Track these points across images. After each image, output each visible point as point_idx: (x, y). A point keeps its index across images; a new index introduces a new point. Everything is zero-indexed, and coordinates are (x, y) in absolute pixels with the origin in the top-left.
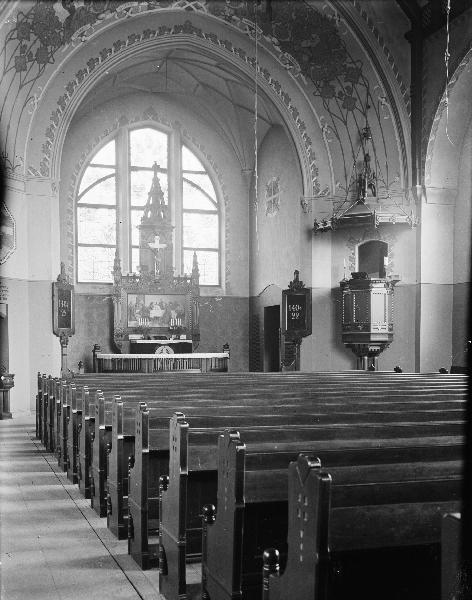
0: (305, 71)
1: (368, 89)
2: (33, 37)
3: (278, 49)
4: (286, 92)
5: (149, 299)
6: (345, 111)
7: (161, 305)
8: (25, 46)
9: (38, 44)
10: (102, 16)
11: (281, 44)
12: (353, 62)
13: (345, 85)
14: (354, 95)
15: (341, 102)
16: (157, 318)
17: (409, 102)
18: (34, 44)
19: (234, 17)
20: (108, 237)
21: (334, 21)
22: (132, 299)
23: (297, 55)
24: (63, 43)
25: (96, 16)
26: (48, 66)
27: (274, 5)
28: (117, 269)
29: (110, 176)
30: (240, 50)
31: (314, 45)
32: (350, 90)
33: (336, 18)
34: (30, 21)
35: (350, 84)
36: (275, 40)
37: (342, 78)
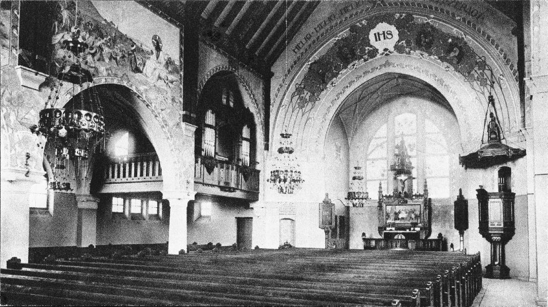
0: (456, 69)
1: (492, 71)
2: (306, 92)
3: (439, 61)
4: (416, 66)
5: (398, 208)
6: (482, 87)
7: (405, 211)
8: (302, 97)
9: (309, 94)
10: (340, 73)
11: (440, 58)
12: (480, 58)
13: (479, 72)
14: (485, 77)
15: (479, 83)
16: (403, 218)
17: (517, 74)
18: (307, 95)
19: (412, 52)
20: (383, 175)
21: (463, 38)
22: (389, 208)
23: (450, 62)
24: (323, 90)
25: (338, 74)
26: (317, 102)
27: (414, 194)
28: (380, 192)
29: (384, 143)
30: (426, 70)
31: (457, 54)
32: (482, 74)
33: (464, 36)
34: (303, 86)
35: (481, 71)
36: (436, 57)
37: (476, 68)
